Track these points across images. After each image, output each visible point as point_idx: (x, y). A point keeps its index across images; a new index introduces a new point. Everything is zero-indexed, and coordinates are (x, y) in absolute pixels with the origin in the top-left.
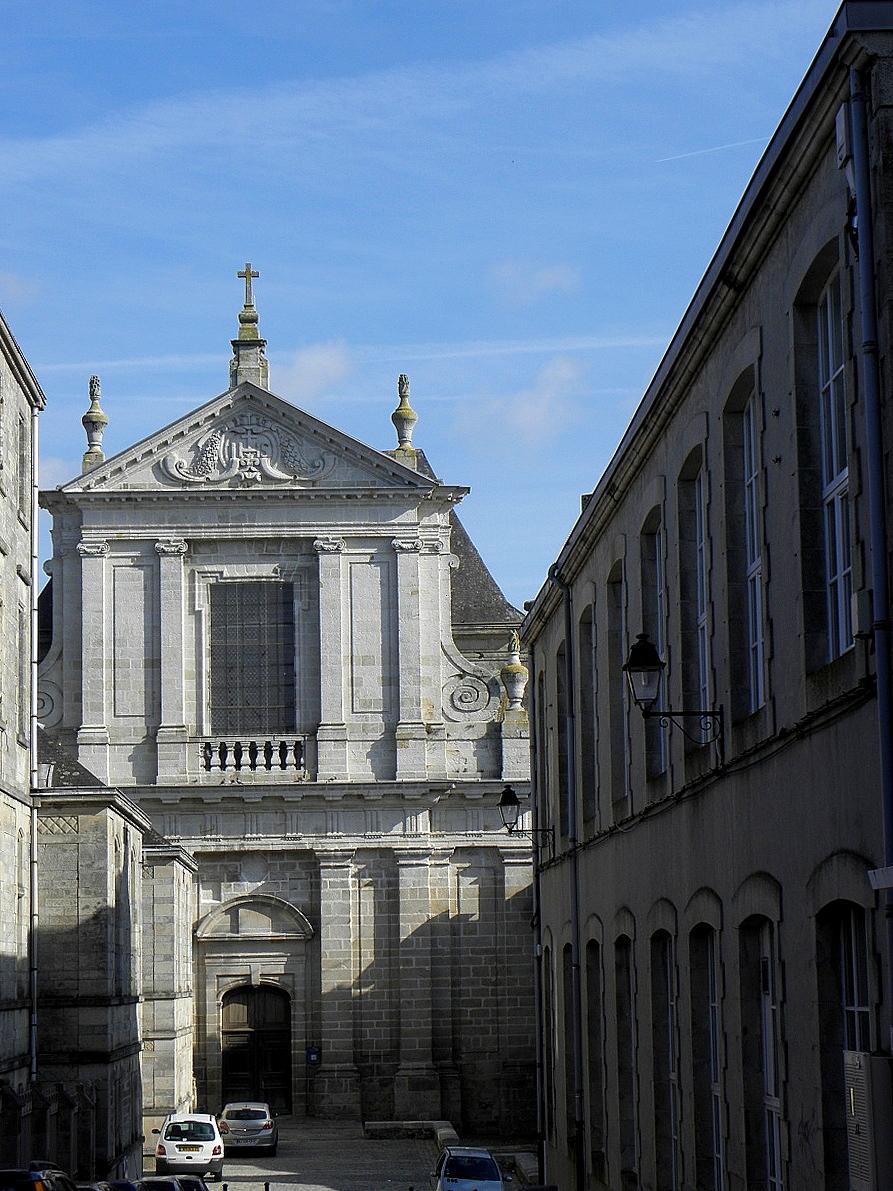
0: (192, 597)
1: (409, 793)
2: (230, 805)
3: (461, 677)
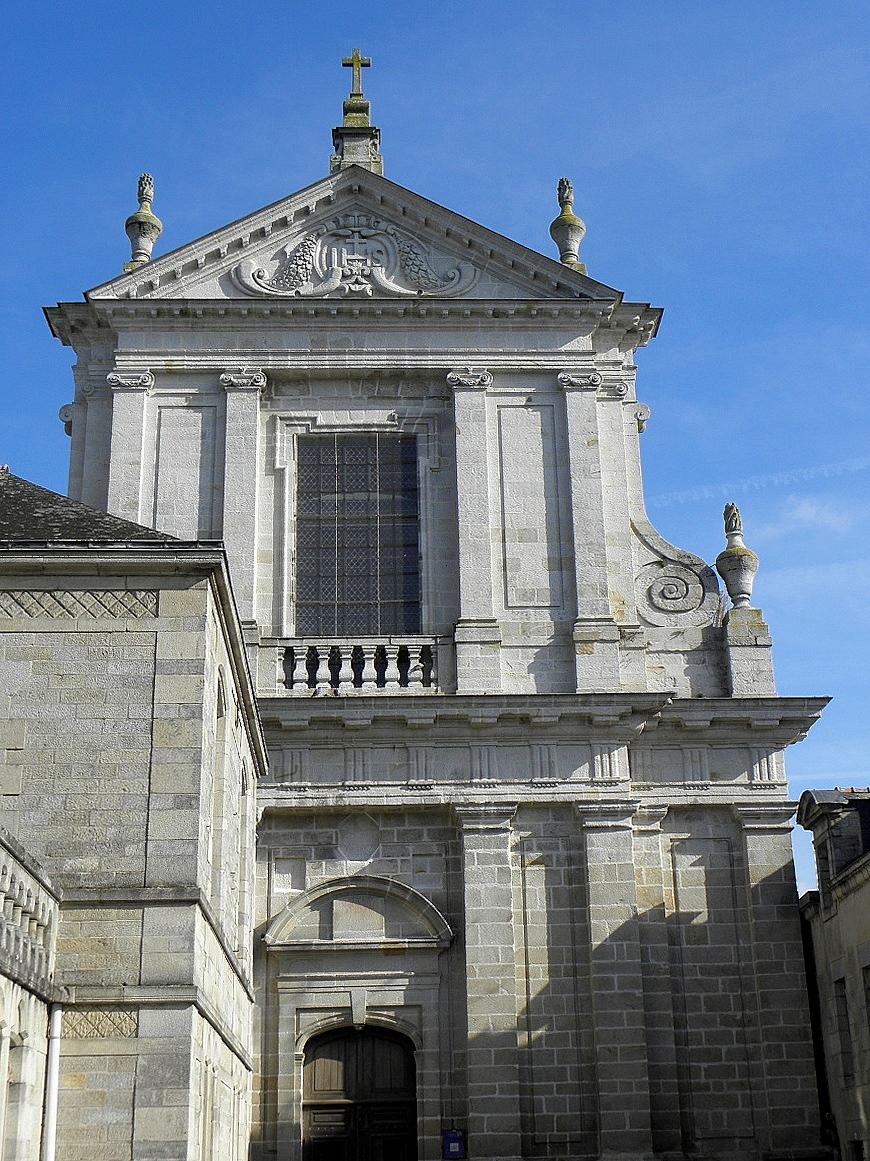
0: (271, 452)
1: (602, 713)
2: (322, 734)
3: (660, 564)
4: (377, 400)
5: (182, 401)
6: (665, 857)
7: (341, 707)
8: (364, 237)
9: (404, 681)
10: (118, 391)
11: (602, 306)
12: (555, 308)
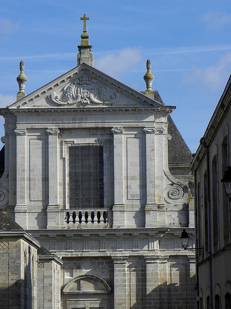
0: (61, 152)
1: (151, 233)
2: (77, 238)
3: (172, 185)
6: (168, 268)
8: (87, 84)
9: (99, 221)
10: (18, 135)
11: (157, 108)
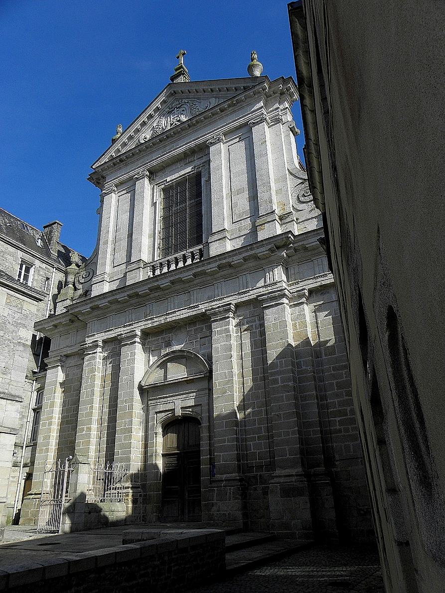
4: (187, 165)
5: (125, 192)
7: (157, 281)
12: (242, 97)
